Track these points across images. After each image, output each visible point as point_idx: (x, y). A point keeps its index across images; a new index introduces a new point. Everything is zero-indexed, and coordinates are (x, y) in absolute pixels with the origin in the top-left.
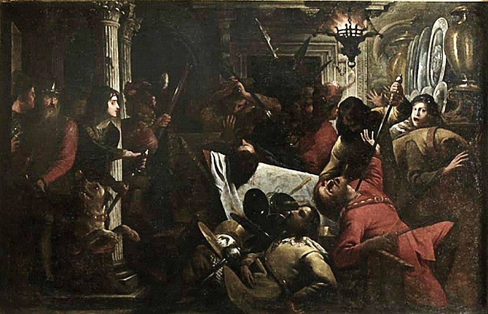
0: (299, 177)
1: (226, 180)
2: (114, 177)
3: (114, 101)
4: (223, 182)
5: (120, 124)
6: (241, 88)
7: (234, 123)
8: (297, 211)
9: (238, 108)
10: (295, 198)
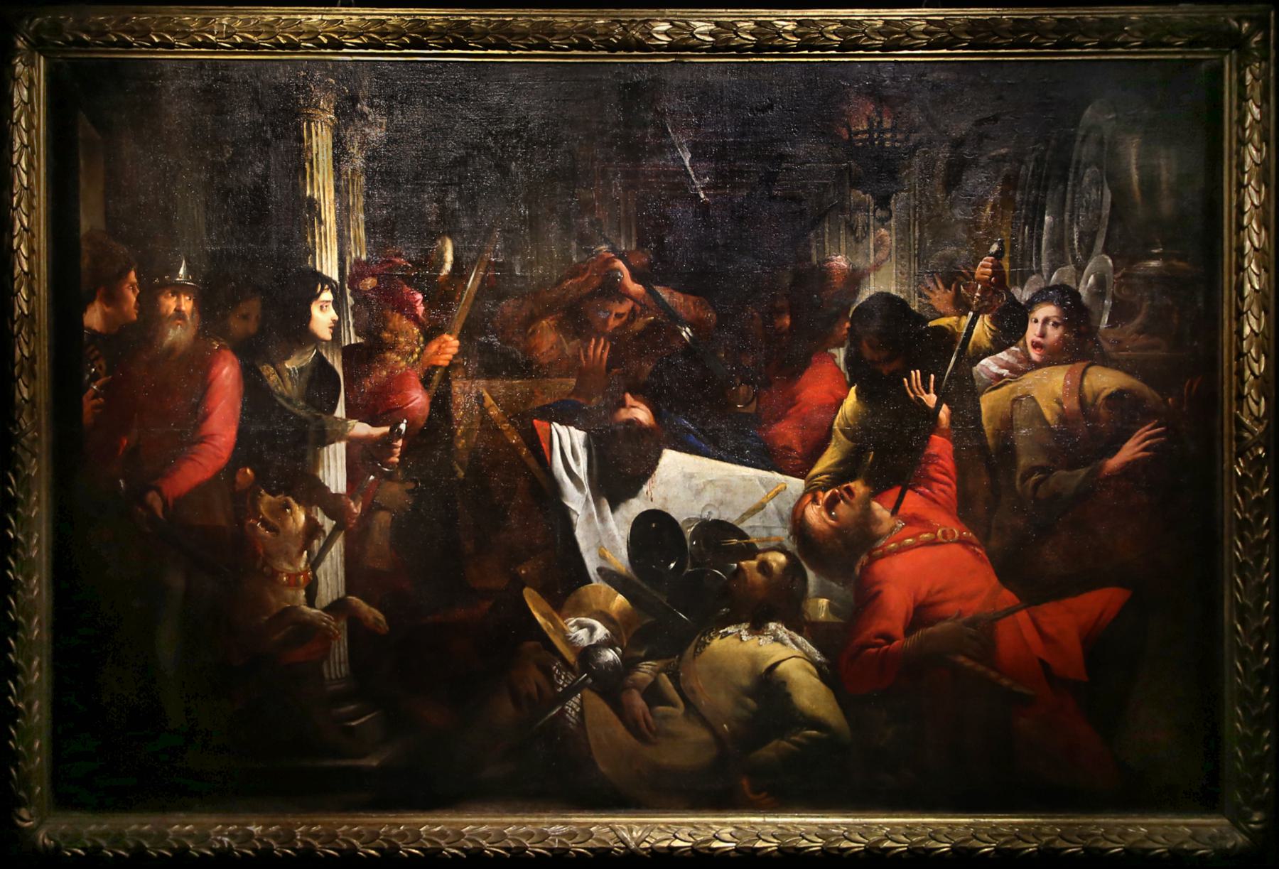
0: (758, 483)
1: (587, 490)
2: (327, 484)
3: (327, 302)
5: (340, 357)
6: (622, 273)
7: (605, 356)
8: (754, 563)
9: (614, 320)
10: (748, 532)
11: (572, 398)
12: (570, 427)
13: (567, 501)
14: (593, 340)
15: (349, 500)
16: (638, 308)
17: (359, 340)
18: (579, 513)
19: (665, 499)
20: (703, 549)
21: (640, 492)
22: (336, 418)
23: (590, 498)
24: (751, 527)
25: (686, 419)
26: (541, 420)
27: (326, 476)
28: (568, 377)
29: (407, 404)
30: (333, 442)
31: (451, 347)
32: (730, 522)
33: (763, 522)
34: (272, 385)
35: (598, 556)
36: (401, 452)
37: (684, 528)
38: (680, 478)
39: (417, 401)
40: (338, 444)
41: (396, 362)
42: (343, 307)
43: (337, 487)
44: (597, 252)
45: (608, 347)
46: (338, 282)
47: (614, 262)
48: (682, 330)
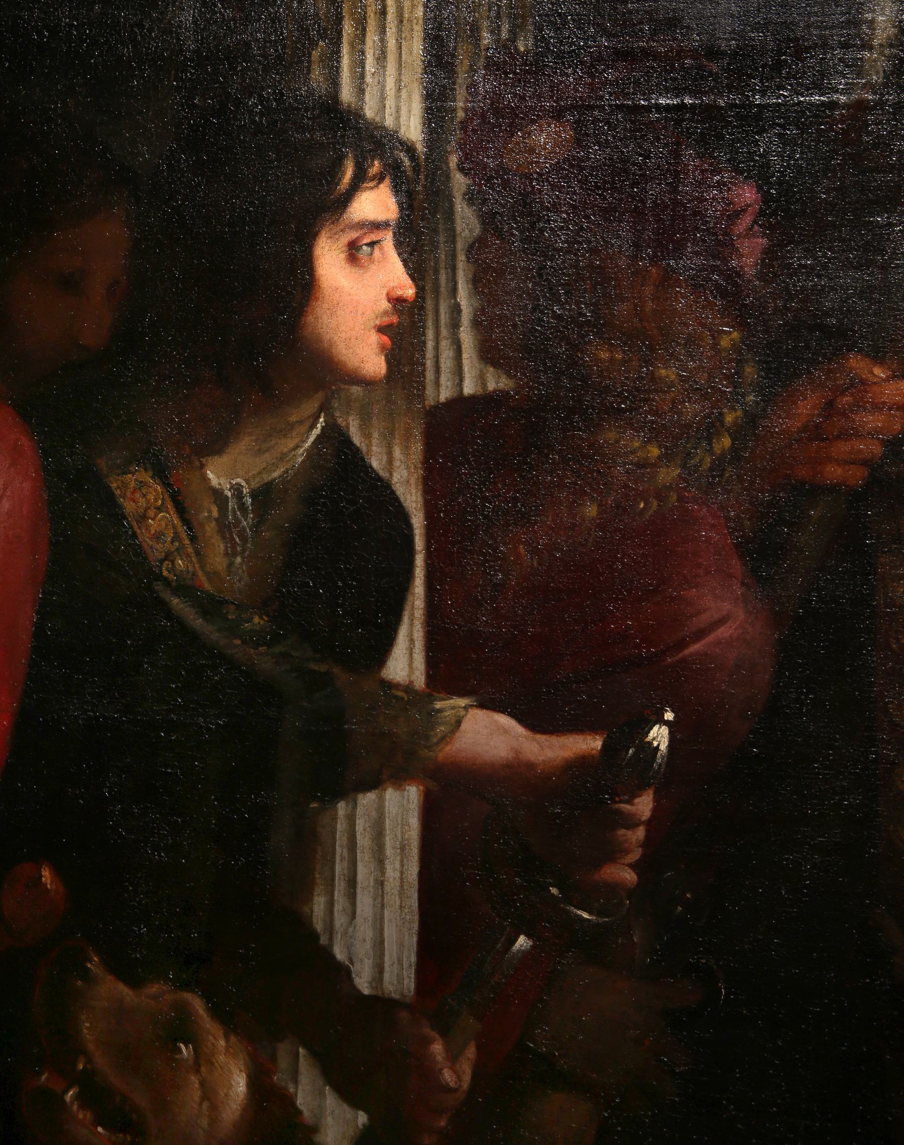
2: (339, 953)
3: (376, 226)
5: (417, 447)
15: (427, 1031)
17: (495, 382)
22: (388, 685)
27: (340, 920)
29: (682, 644)
30: (374, 783)
31: (877, 407)
34: (155, 551)
36: (646, 844)
39: (723, 632)
40: (390, 794)
41: (642, 464)
42: (435, 246)
43: (379, 968)
46: (420, 148)
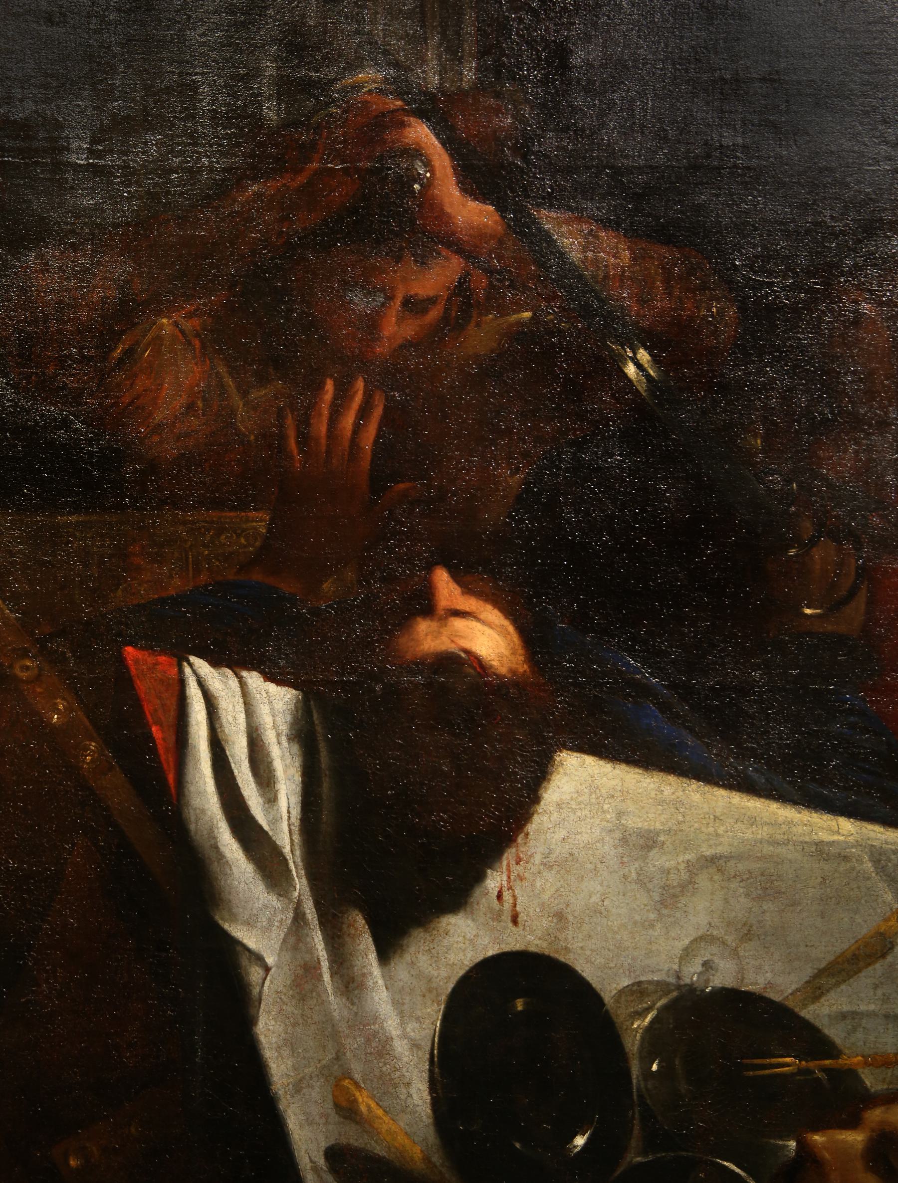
0: (869, 866)
1: (300, 884)
4: (273, 900)
6: (428, 164)
7: (368, 441)
8: (855, 1138)
9: (400, 321)
10: (835, 1033)
11: (257, 576)
12: (244, 674)
13: (234, 918)
14: (329, 386)
16: (479, 283)
18: (270, 960)
19: (560, 916)
20: (683, 1087)
21: (477, 892)
23: (309, 908)
24: (843, 1016)
25: (631, 651)
26: (149, 648)
28: (244, 506)
32: (777, 997)
33: (886, 999)
35: (329, 1105)
37: (620, 1014)
38: (608, 849)
44: (345, 91)
45: (378, 412)
47: (403, 125)
48: (623, 359)
